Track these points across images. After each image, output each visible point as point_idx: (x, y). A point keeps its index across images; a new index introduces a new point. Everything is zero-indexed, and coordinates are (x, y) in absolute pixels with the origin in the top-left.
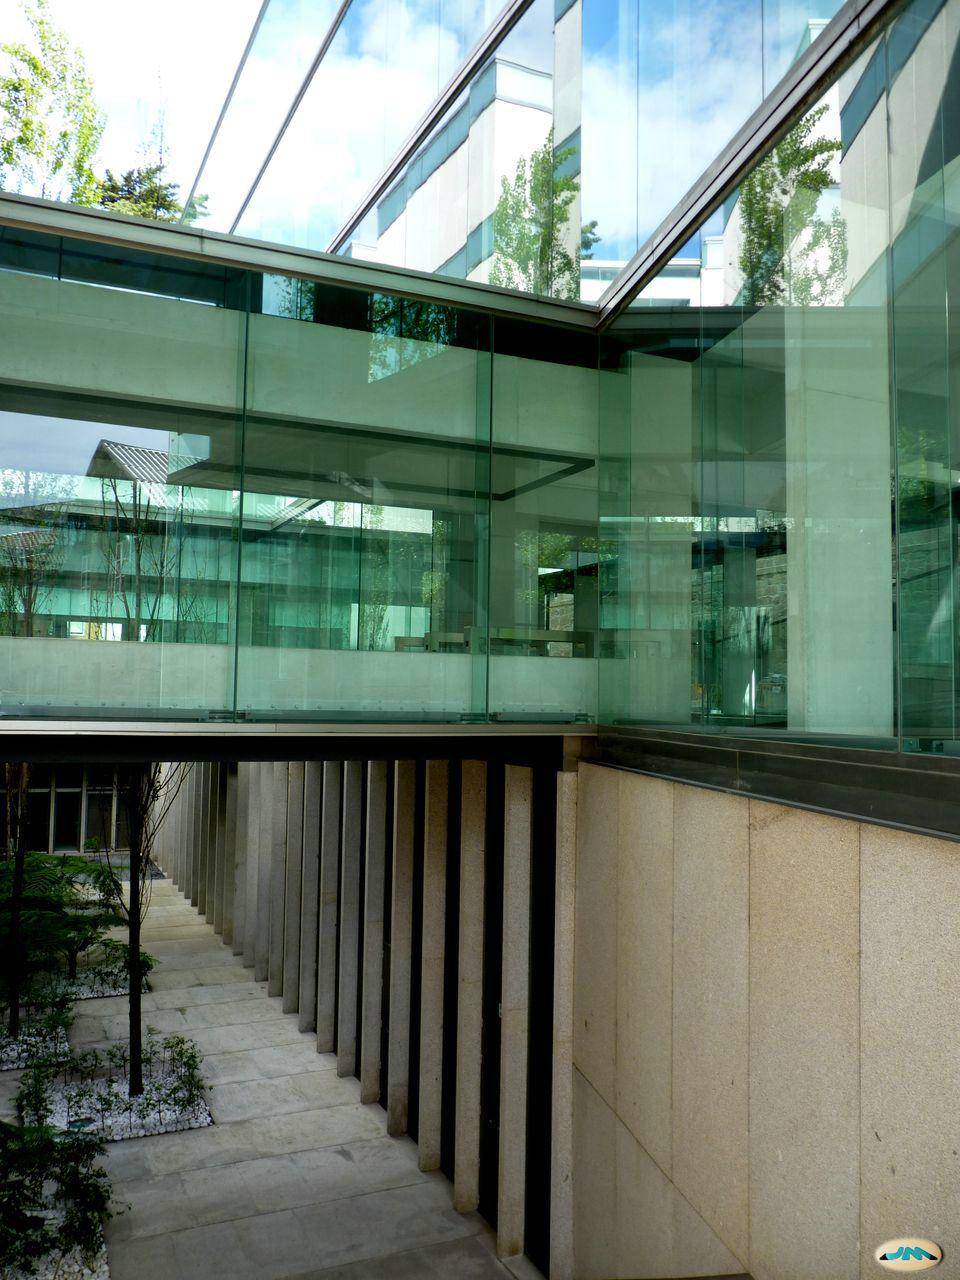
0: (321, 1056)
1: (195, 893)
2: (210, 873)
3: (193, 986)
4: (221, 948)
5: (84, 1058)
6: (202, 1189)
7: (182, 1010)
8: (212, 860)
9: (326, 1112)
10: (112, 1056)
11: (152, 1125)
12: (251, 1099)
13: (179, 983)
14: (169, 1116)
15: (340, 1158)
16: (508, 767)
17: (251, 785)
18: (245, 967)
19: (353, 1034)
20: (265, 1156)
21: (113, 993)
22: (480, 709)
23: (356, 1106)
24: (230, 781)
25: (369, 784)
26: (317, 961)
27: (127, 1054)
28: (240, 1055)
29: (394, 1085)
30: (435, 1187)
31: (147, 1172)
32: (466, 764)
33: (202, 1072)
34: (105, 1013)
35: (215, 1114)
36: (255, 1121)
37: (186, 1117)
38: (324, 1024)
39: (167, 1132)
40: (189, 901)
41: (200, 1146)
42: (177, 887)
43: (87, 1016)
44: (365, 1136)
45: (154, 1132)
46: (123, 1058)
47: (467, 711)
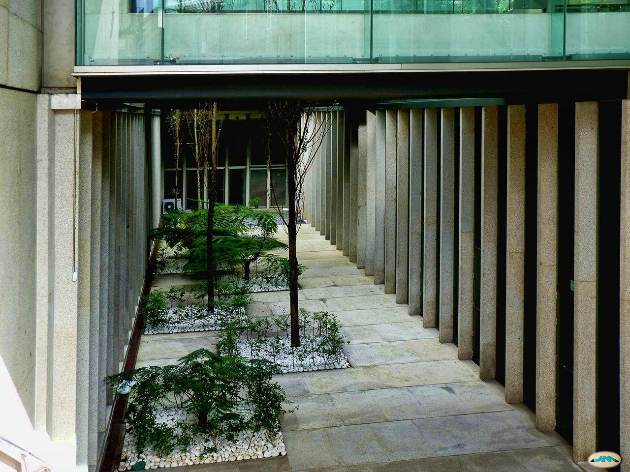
0: (426, 330)
1: (328, 231)
2: (339, 218)
3: (330, 286)
4: (348, 264)
5: (259, 323)
6: (344, 404)
7: (324, 300)
8: (340, 191)
9: (433, 363)
10: (278, 323)
11: (308, 365)
12: (376, 353)
13: (320, 284)
14: (319, 360)
15: (445, 392)
16: (577, 104)
17: (368, 151)
18: (367, 276)
19: (451, 313)
20: (388, 387)
21: (275, 289)
22: (558, 51)
23: (455, 361)
24: (353, 151)
25: (461, 135)
26: (422, 266)
27: (289, 322)
28: (366, 327)
29: (485, 345)
30: (520, 416)
31: (307, 392)
32: (542, 108)
33: (341, 333)
34: (270, 301)
35: (352, 361)
36: (380, 366)
37: (331, 362)
38: (428, 309)
39: (318, 370)
40: (324, 237)
41: (342, 379)
42: (314, 228)
43: (259, 302)
44: (463, 379)
45: (310, 370)
46: (286, 325)
47: (547, 55)
